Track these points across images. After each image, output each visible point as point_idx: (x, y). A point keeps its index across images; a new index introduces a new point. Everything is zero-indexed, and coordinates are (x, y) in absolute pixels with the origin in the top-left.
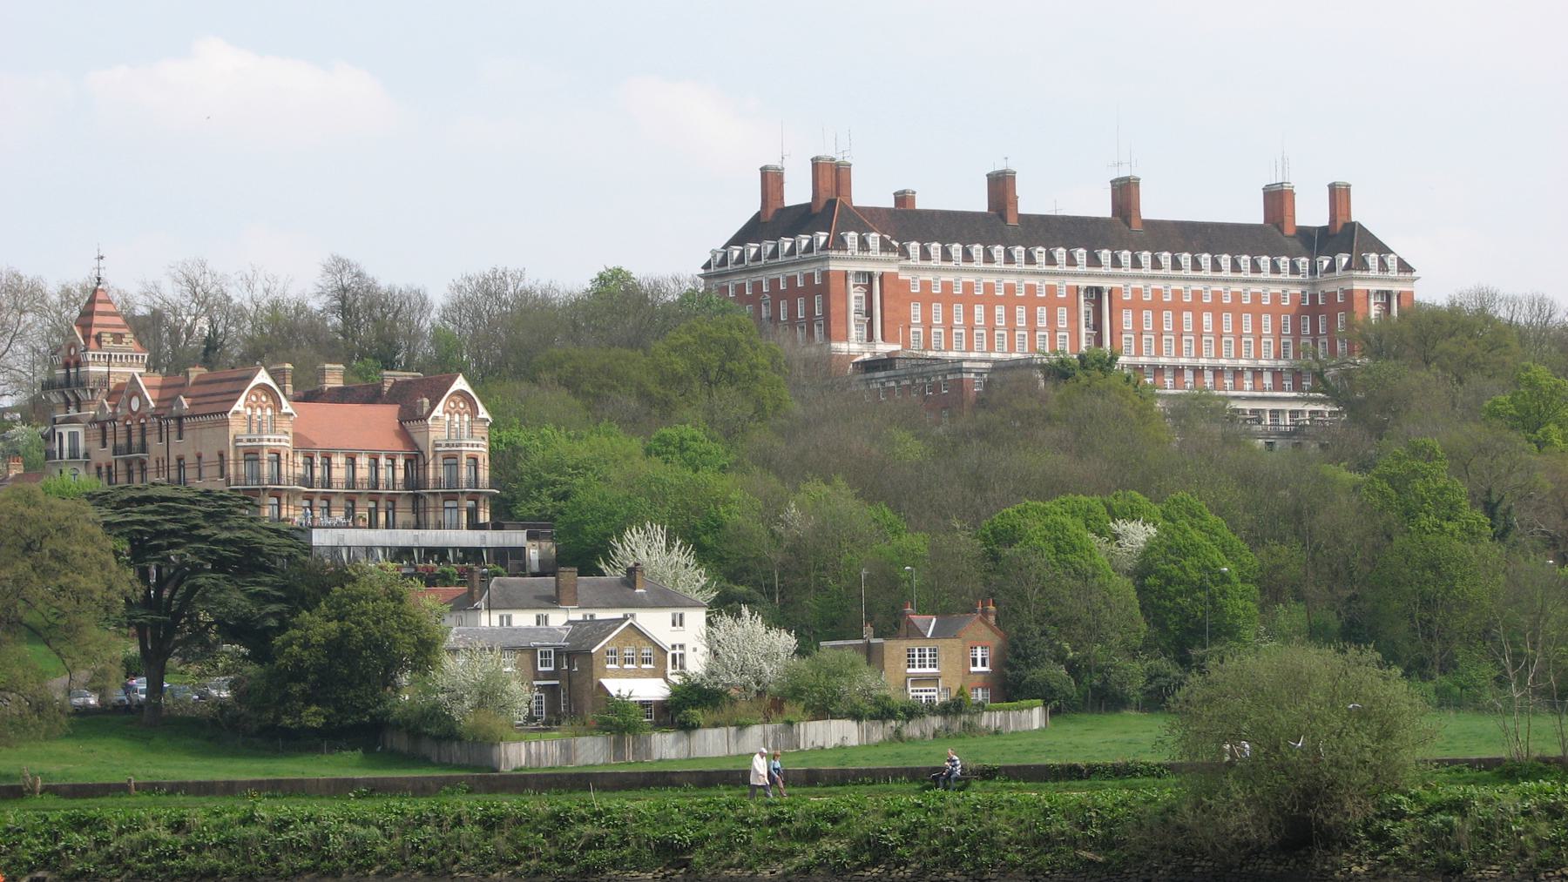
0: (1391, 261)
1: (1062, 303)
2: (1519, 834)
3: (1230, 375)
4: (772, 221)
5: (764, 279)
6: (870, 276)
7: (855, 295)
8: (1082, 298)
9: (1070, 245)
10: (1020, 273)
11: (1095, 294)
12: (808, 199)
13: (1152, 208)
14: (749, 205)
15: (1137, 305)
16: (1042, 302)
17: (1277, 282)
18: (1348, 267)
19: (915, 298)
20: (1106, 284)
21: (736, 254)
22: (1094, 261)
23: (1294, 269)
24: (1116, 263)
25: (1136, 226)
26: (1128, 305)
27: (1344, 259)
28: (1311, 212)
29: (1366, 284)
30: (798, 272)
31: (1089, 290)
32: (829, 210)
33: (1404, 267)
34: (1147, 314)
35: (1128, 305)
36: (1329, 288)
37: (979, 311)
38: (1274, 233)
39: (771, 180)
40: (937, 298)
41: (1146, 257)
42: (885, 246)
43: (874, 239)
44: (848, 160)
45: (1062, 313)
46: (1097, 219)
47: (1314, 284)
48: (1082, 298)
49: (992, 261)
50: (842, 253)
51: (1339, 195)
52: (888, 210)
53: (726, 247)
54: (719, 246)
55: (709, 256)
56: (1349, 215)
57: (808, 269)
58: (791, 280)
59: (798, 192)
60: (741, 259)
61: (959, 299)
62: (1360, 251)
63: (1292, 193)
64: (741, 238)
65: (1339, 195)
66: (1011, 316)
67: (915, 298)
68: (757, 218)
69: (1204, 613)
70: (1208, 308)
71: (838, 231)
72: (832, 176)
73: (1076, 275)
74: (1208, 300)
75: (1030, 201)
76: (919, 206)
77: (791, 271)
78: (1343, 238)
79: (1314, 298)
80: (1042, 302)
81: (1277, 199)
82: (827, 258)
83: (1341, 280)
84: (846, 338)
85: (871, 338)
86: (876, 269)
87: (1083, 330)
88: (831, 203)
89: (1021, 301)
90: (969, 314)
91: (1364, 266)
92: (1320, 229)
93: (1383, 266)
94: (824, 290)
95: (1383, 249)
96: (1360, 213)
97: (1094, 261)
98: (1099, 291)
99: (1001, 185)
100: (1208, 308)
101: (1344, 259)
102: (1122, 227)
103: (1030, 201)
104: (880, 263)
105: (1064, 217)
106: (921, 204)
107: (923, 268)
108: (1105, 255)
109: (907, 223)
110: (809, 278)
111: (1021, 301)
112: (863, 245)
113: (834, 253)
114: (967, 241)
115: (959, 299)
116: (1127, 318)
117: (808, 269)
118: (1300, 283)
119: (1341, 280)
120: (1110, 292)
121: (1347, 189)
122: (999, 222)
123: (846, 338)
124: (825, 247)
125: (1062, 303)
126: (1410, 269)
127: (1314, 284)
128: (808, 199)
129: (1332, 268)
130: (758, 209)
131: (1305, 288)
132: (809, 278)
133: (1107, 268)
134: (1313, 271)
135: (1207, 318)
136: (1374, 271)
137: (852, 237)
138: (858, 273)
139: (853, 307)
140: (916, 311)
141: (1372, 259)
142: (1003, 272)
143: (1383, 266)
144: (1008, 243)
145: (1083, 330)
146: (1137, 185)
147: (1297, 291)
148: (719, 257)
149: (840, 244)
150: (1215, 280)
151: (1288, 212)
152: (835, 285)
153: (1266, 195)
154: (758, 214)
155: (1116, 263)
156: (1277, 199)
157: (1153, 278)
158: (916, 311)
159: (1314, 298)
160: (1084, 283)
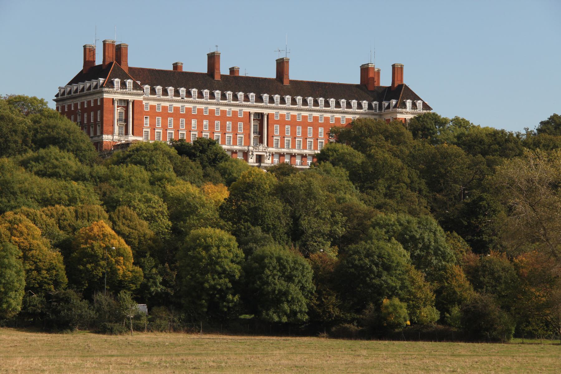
0: (419, 103)
1: (240, 120)
3: (300, 157)
5: (79, 101)
6: (127, 102)
7: (118, 111)
8: (252, 118)
10: (218, 104)
11: (260, 117)
13: (295, 74)
14: (78, 67)
15: (282, 122)
19: (147, 113)
20: (266, 111)
23: (360, 106)
24: (271, 100)
25: (286, 83)
26: (277, 122)
28: (386, 81)
31: (256, 114)
34: (159, 119)
35: (277, 122)
37: (194, 122)
39: (88, 52)
42: (136, 87)
43: (129, 82)
44: (288, 57)
45: (241, 125)
46: (265, 79)
48: (252, 118)
49: (340, 107)
50: (404, 110)
51: (397, 70)
52: (170, 71)
56: (402, 80)
61: (183, 116)
63: (126, 47)
64: (77, 80)
65: (397, 70)
68: (81, 72)
69: (104, 274)
71: (110, 78)
72: (119, 51)
76: (184, 70)
78: (399, 92)
82: (102, 92)
84: (112, 133)
85: (127, 133)
86: (130, 98)
87: (252, 135)
90: (189, 124)
92: (386, 88)
94: (101, 108)
95: (415, 98)
96: (408, 81)
97: (259, 99)
98: (262, 115)
99: (282, 65)
105: (249, 77)
106: (241, 74)
108: (266, 96)
111: (218, 118)
112: (123, 85)
116: (277, 127)
120: (268, 116)
121: (402, 68)
123: (112, 133)
124: (395, 106)
125: (240, 120)
126: (429, 108)
127: (381, 115)
130: (82, 68)
137: (117, 81)
138: (121, 100)
139: (116, 117)
141: (409, 103)
143: (414, 106)
145: (252, 135)
146: (288, 62)
150: (326, 112)
151: (217, 66)
152: (106, 106)
153: (361, 69)
154: (82, 71)
160: (253, 110)
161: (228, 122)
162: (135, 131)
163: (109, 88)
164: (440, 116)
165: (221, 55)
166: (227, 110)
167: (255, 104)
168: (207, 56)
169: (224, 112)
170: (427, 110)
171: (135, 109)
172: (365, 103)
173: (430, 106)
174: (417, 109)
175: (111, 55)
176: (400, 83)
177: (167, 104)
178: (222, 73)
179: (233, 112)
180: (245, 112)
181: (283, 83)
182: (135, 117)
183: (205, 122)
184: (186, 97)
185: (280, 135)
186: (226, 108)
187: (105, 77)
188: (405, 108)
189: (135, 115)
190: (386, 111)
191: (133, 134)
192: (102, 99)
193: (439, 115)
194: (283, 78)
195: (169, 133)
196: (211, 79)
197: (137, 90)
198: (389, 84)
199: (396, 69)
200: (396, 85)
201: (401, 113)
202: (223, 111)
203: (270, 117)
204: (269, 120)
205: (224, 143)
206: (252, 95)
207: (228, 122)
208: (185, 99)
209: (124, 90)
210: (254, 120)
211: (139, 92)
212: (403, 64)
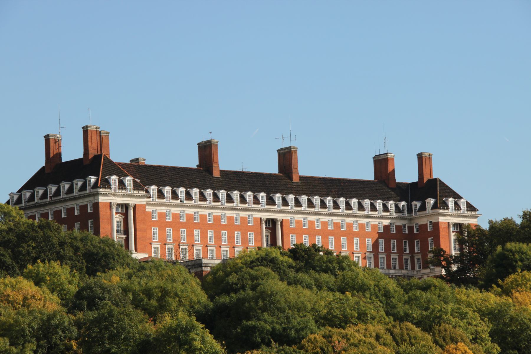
0: (462, 203)
1: (251, 229)
2: (114, 323)
4: (54, 170)
6: (126, 207)
9: (256, 190)
10: (223, 209)
11: (272, 224)
12: (81, 156)
13: (306, 167)
15: (162, 224)
16: (238, 228)
17: (379, 217)
18: (435, 207)
19: (155, 224)
21: (28, 194)
22: (271, 201)
23: (386, 209)
24: (285, 203)
25: (296, 179)
27: (431, 201)
28: (406, 173)
29: (448, 218)
30: (75, 205)
31: (268, 221)
32: (94, 165)
33: (470, 207)
36: (422, 222)
38: (382, 183)
40: (169, 225)
41: (304, 199)
42: (136, 186)
43: (129, 180)
44: (294, 145)
46: (270, 175)
47: (410, 220)
52: (270, 175)
53: (20, 191)
54: (16, 190)
55: (8, 198)
56: (431, 174)
57: (82, 202)
58: (70, 211)
59: (72, 151)
60: (32, 198)
61: (184, 225)
62: (442, 197)
64: (30, 185)
65: (423, 161)
66: (218, 237)
67: (155, 224)
70: (344, 234)
71: (104, 175)
73: (259, 211)
74: (343, 229)
75: (226, 161)
77: (69, 205)
78: (429, 190)
79: (411, 228)
80: (238, 228)
81: (382, 163)
82: (97, 194)
83: (431, 215)
88: (98, 158)
89: (224, 227)
91: (445, 206)
93: (457, 206)
95: (457, 196)
96: (438, 172)
97: (271, 201)
100: (344, 234)
101: (431, 201)
102: (284, 180)
103: (226, 161)
104: (134, 199)
107: (157, 205)
108: (278, 197)
109: (148, 175)
110: (83, 208)
111: (224, 227)
112: (122, 185)
113: (101, 190)
114: (189, 186)
115: (184, 225)
117: (82, 202)
118: (403, 219)
119: (431, 215)
120: (282, 223)
122: (204, 175)
124: (95, 186)
125: (251, 229)
126: (475, 210)
127: (410, 220)
128: (81, 156)
129: (423, 208)
130: (43, 164)
131: (405, 222)
132: (83, 208)
133: (279, 206)
134: (410, 210)
135: (237, 234)
136: (451, 210)
137: (114, 179)
138: (119, 205)
140: (155, 231)
141: (451, 201)
142: (212, 208)
143: (457, 206)
144: (216, 188)
146: (296, 152)
147: (387, 222)
148: (16, 197)
149: (107, 184)
150: (348, 216)
151: (214, 158)
152: (103, 213)
153: (375, 161)
155: (285, 203)
156: (382, 163)
157: (309, 213)
158: (155, 231)
159: (411, 228)
161: (236, 232)
162: (138, 246)
163: (106, 188)
164: (496, 222)
165: (219, 144)
166: (235, 216)
167: (266, 207)
168: (197, 147)
169: (230, 219)
170: (472, 211)
171: (137, 216)
172: (391, 204)
173: (475, 207)
174: (126, 189)
175: (94, 146)
176: (430, 178)
177: (163, 210)
178: (221, 168)
179: (241, 218)
180: (255, 219)
181: (291, 180)
182: (137, 227)
183: (210, 233)
184: (186, 199)
185: (215, 244)
186: (233, 214)
187: (96, 174)
188: (448, 208)
189: (137, 224)
190: (418, 213)
191: (136, 250)
192: (96, 206)
193: (510, 218)
194: (211, 166)
195: (154, 248)
196: (209, 175)
197: (139, 190)
198: (79, 154)
199: (89, 133)
200: (91, 156)
201: (444, 215)
202: (230, 217)
203: (284, 224)
204: (284, 228)
205: (206, 257)
206: (262, 196)
207: (236, 232)
208: (185, 202)
209: (123, 191)
210: (266, 228)
211: (141, 192)
212: (431, 153)
